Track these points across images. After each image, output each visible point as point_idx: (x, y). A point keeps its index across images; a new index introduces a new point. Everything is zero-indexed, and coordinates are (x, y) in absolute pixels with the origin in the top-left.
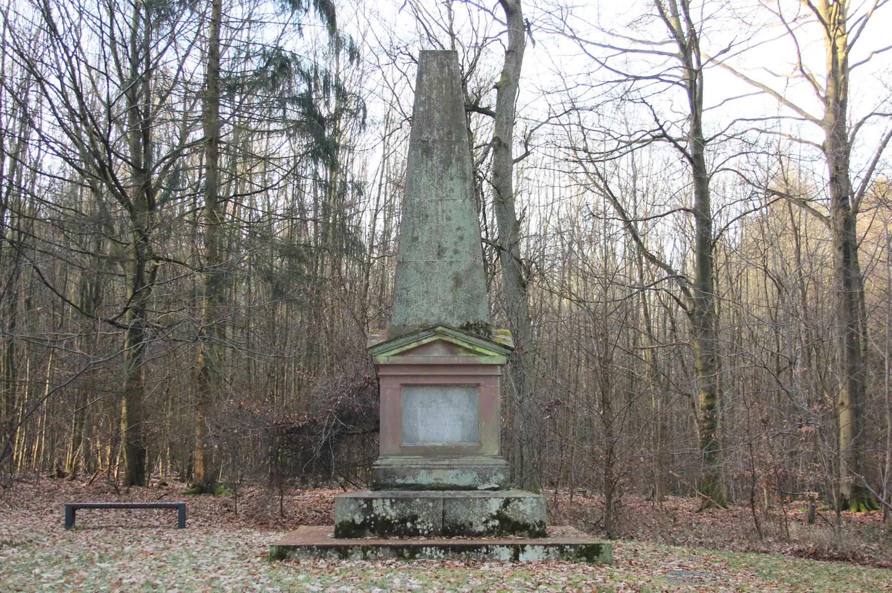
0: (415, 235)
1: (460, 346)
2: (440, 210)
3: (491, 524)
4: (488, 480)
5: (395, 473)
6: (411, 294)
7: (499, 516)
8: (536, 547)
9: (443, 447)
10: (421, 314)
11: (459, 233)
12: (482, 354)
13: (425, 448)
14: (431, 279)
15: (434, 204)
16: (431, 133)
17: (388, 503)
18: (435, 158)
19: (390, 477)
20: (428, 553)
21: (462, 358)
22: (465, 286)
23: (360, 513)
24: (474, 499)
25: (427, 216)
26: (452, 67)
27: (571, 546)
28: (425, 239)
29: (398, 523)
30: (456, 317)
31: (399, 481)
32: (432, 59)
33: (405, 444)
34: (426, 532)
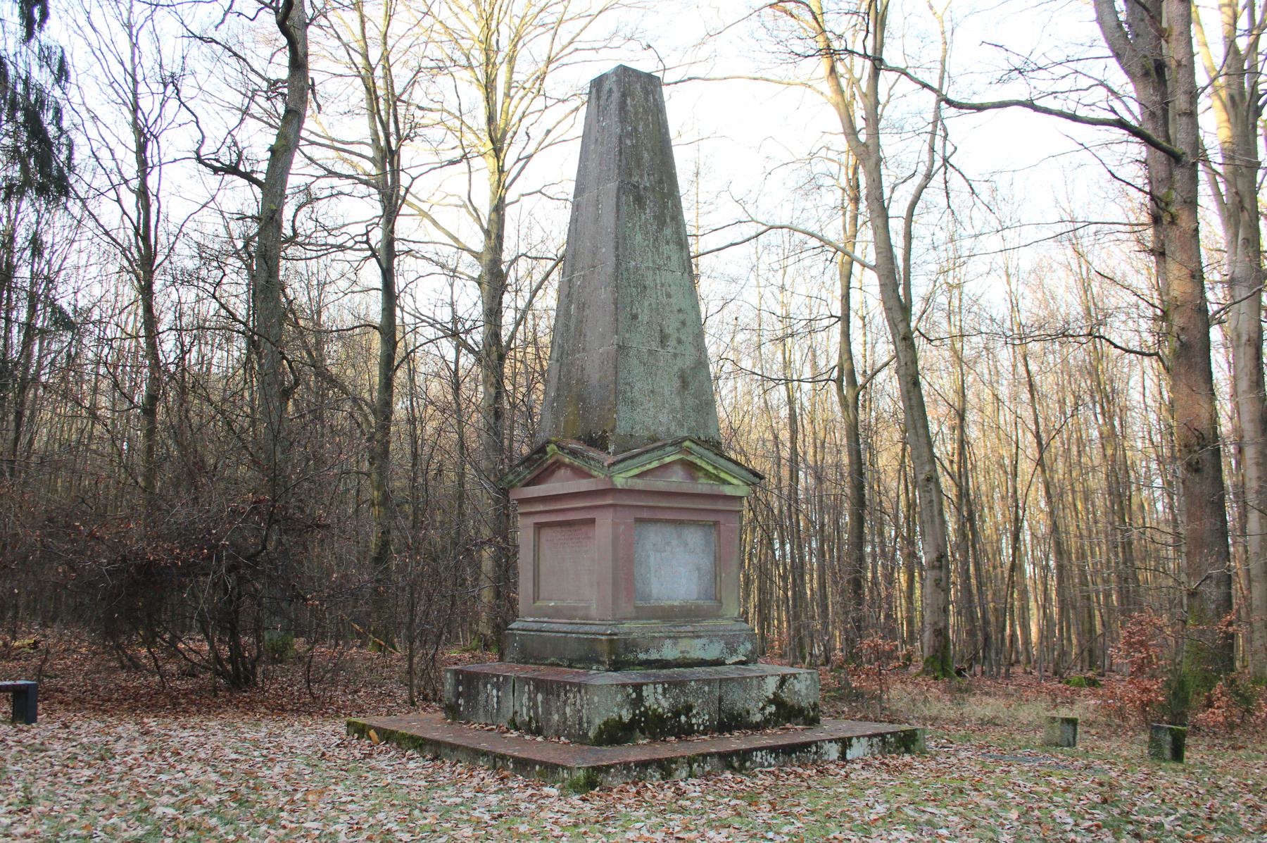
1: (701, 469)
3: (767, 712)
4: (736, 651)
5: (636, 646)
6: (636, 394)
7: (776, 700)
10: (649, 421)
11: (681, 317)
12: (725, 482)
13: (662, 608)
16: (641, 176)
17: (660, 690)
20: (758, 760)
21: (703, 485)
22: (692, 388)
24: (751, 678)
27: (891, 733)
28: (646, 319)
29: (670, 718)
31: (642, 656)
33: (640, 603)
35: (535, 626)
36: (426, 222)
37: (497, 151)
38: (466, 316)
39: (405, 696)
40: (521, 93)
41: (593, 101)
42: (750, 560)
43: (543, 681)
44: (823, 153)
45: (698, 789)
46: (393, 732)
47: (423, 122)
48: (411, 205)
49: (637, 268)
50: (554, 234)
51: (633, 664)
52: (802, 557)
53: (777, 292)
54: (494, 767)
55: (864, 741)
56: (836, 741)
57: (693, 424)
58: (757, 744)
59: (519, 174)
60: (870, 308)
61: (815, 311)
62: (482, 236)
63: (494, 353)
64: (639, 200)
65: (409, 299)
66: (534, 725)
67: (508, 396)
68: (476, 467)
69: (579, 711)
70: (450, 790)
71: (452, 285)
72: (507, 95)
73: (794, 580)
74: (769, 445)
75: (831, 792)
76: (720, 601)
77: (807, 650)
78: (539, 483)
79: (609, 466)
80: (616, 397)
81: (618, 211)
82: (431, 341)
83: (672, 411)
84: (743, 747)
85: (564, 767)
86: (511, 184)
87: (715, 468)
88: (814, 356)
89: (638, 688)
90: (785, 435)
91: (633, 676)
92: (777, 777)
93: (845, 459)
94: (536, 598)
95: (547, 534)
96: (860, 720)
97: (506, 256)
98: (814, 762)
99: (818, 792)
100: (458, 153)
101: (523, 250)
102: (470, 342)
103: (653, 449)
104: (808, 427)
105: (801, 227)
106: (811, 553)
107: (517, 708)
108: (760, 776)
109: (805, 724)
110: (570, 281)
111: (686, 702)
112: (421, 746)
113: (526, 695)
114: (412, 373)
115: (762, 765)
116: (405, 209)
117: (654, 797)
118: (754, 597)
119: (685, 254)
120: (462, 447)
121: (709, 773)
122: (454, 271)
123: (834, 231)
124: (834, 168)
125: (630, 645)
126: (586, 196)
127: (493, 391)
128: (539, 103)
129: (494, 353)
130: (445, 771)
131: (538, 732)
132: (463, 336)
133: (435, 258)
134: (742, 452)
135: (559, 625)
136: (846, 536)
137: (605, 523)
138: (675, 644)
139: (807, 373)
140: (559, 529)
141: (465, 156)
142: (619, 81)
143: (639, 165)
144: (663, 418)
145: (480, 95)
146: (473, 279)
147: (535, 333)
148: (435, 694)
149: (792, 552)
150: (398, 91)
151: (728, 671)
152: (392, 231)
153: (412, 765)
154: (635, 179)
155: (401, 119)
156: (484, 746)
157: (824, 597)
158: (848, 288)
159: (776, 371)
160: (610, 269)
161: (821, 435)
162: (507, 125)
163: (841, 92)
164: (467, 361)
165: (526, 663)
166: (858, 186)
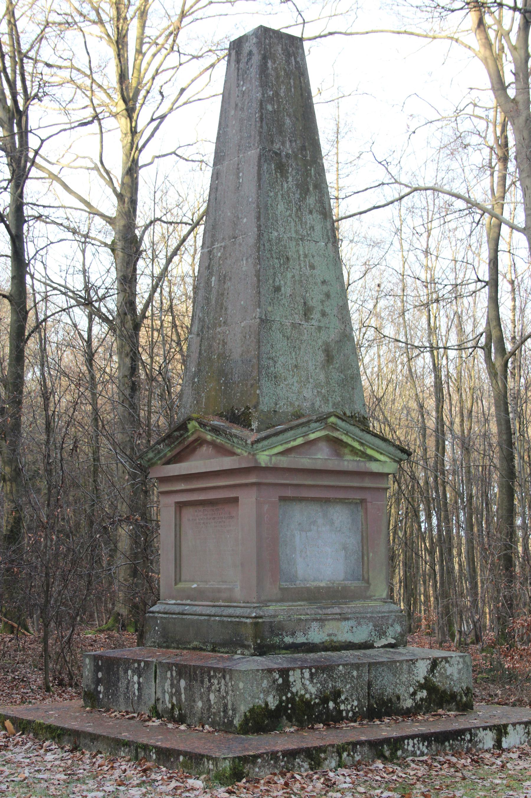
0: (277, 284)
1: (346, 445)
2: (301, 253)
3: (418, 697)
4: (384, 633)
6: (279, 369)
7: (427, 685)
8: (517, 726)
9: (328, 589)
11: (325, 288)
13: (308, 589)
14: (300, 349)
15: (294, 243)
16: (283, 143)
17: (307, 675)
18: (290, 179)
19: (277, 635)
20: (410, 748)
21: (349, 462)
22: (337, 363)
23: (274, 693)
24: (401, 662)
25: (288, 258)
26: (298, 59)
28: (289, 291)
30: (331, 404)
31: (288, 640)
32: (276, 41)
33: (284, 585)
34: (350, 714)
35: (177, 609)
36: (56, 184)
37: (130, 112)
38: (98, 283)
39: (40, 682)
40: (154, 49)
41: (233, 64)
42: (395, 533)
43: (185, 666)
44: (469, 110)
45: (348, 779)
46: (29, 722)
47: (52, 80)
48: (40, 168)
49: (279, 239)
50: (191, 198)
51: (279, 648)
52: (449, 531)
53: (422, 256)
54: (136, 758)
55: (520, 728)
56: (491, 728)
57: (339, 399)
58: (409, 731)
59: (152, 135)
60: (519, 271)
61: (461, 275)
62: (115, 200)
63: (128, 321)
64: (281, 168)
65: (39, 266)
66: (176, 713)
67: (144, 367)
68: (110, 437)
69: (224, 698)
70: (91, 784)
71: (83, 251)
72: (139, 51)
73: (441, 554)
74: (415, 414)
75: (487, 783)
76: (368, 582)
77: (456, 627)
78: (175, 462)
79: (252, 444)
80: (259, 373)
81: (259, 179)
82: (64, 310)
83: (316, 386)
84: (395, 734)
85: (209, 758)
86: (144, 146)
87: (362, 444)
88: (460, 324)
89: (284, 673)
90: (431, 404)
91: (278, 661)
92: (430, 767)
93: (494, 428)
94: (178, 579)
95: (188, 514)
96: (514, 705)
97: (140, 221)
98: (469, 751)
99: (473, 783)
100: (88, 113)
101: (158, 216)
102: (104, 310)
103: (298, 426)
104: (455, 397)
105: (447, 188)
106: (459, 526)
107: (159, 695)
108: (413, 765)
109: (458, 709)
110: (210, 252)
111: (334, 687)
112: (59, 736)
113: (169, 682)
114: (43, 342)
115: (414, 754)
116: (34, 172)
117: (303, 788)
118: (400, 573)
119: (328, 224)
120: (96, 420)
121: (359, 762)
122: (86, 236)
123: (481, 190)
124: (482, 125)
125: (276, 629)
126: (226, 163)
127: (128, 361)
128: (173, 59)
129: (128, 321)
130: (85, 765)
131: (181, 720)
132: (96, 305)
133: (66, 223)
134: (386, 421)
135: (202, 608)
136: (495, 508)
137: (248, 501)
138: (322, 627)
139: (453, 340)
140: (201, 508)
141: (96, 117)
142: (259, 44)
143: (280, 132)
144: (308, 393)
145: (111, 52)
146: (106, 245)
147: (171, 300)
148: (71, 679)
149: (439, 525)
150: (24, 48)
151: (377, 655)
152: (21, 196)
153: (49, 757)
154: (277, 146)
155: (28, 78)
156: (125, 736)
157: (473, 570)
158: (496, 251)
159: (420, 338)
160: (251, 240)
161: (468, 404)
162: (139, 83)
163: (489, 45)
164: (99, 329)
165: (168, 647)
166: (506, 145)
